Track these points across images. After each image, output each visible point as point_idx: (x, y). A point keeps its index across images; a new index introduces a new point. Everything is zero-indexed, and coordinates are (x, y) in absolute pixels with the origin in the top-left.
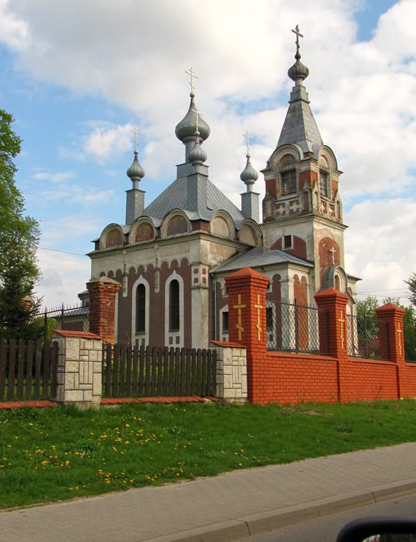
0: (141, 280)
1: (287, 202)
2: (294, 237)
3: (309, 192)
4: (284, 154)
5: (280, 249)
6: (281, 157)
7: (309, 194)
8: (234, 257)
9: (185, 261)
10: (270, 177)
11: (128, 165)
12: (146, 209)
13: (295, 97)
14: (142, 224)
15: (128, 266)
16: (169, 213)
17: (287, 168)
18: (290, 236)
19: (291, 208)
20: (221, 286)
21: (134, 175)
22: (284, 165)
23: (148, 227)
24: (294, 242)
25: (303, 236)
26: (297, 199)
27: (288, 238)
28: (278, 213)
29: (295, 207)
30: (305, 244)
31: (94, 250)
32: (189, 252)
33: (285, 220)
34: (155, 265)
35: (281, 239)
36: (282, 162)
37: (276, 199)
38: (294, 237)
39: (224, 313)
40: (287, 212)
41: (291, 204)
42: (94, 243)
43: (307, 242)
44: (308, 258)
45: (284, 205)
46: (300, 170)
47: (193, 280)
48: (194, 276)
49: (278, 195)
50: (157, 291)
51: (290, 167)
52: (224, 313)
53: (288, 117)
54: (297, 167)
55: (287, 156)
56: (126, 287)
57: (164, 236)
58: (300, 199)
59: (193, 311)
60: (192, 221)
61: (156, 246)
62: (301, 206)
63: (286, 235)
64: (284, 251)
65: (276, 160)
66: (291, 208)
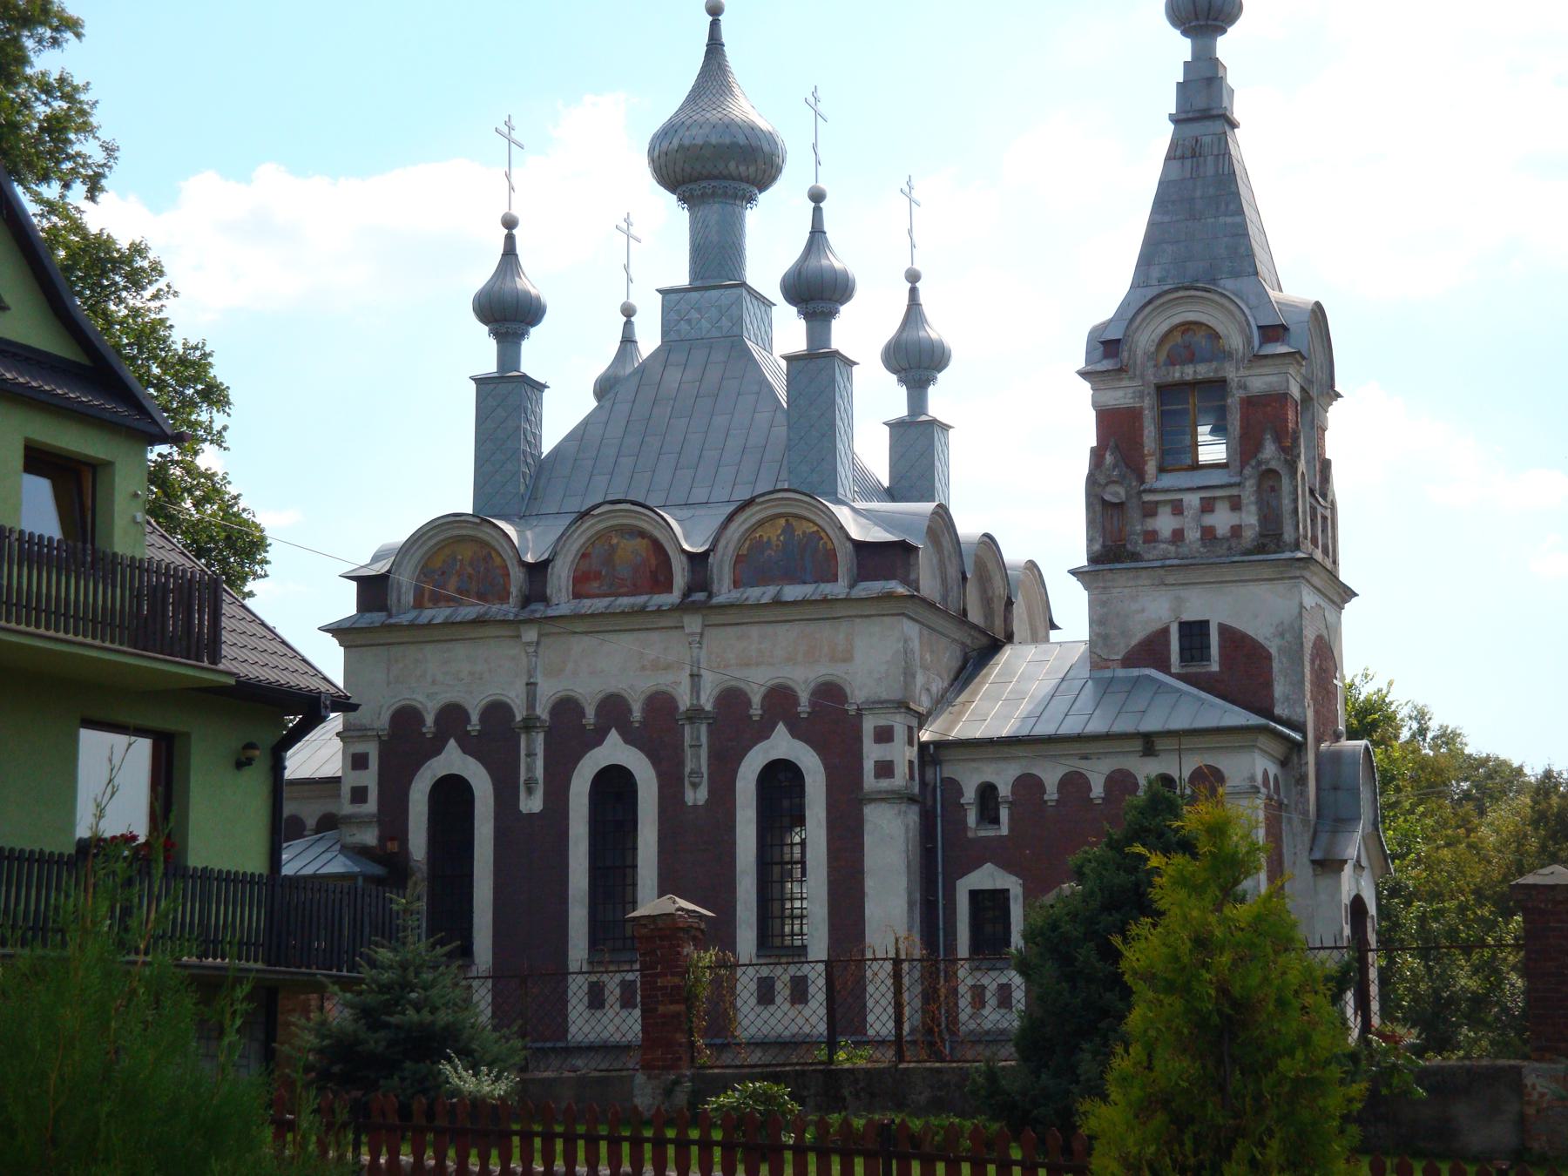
0: (614, 751)
1: (1192, 500)
2: (1220, 625)
3: (1283, 471)
4: (1177, 320)
5: (1164, 667)
6: (1165, 327)
7: (1285, 481)
8: (964, 675)
9: (830, 693)
10: (1120, 397)
11: (481, 273)
12: (556, 451)
13: (1200, 102)
14: (612, 529)
15: (549, 691)
16: (749, 503)
17: (1189, 372)
18: (1204, 625)
19: (1209, 520)
20: (961, 794)
21: (508, 313)
22: (1172, 361)
23: (640, 544)
24: (1221, 647)
25: (1259, 628)
26: (1235, 491)
27: (1194, 633)
28: (1151, 537)
29: (1222, 520)
30: (1269, 657)
31: (352, 609)
32: (848, 658)
33: (1187, 565)
34: (684, 701)
35: (1165, 631)
36: (1166, 348)
37: (1142, 482)
38: (1224, 630)
39: (974, 895)
40: (1193, 535)
41: (1207, 506)
42: (354, 584)
43: (1273, 651)
44: (1278, 711)
45: (1178, 508)
46: (1245, 387)
47: (869, 766)
48: (872, 753)
49: (1151, 467)
50: (696, 796)
51: (1203, 371)
52: (974, 895)
53: (1174, 176)
54: (1231, 373)
55: (1187, 327)
56: (539, 772)
57: (725, 592)
58: (1248, 494)
59: (870, 884)
60: (860, 546)
61: (693, 623)
62: (1250, 518)
63: (1186, 617)
64: (1179, 677)
65: (1146, 339)
66: (1209, 520)
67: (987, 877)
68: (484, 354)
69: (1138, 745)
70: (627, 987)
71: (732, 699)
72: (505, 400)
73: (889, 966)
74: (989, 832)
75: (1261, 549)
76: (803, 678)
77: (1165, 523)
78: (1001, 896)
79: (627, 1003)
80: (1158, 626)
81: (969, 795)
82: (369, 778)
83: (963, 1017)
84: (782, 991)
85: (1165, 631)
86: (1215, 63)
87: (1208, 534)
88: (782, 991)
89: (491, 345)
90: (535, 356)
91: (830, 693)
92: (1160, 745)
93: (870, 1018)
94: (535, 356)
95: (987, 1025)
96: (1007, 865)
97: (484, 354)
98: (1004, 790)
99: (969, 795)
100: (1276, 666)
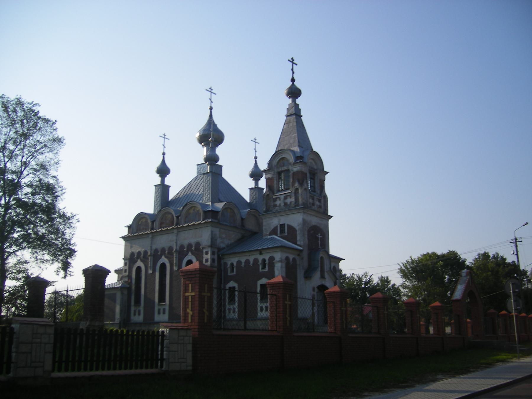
1: (282, 197)
5: (276, 235)
6: (278, 159)
9: (198, 244)
16: (186, 205)
27: (282, 226)
29: (288, 201)
30: (296, 231)
35: (277, 227)
38: (288, 226)
40: (282, 204)
43: (297, 229)
46: (292, 170)
51: (285, 168)
54: (290, 168)
62: (293, 199)
63: (281, 223)
67: (232, 284)
68: (157, 180)
69: (258, 253)
70: (267, 307)
71: (182, 247)
72: (163, 190)
73: (310, 302)
74: (232, 274)
75: (295, 206)
76: (193, 241)
77: (278, 203)
78: (234, 288)
79: (267, 310)
80: (275, 226)
81: (229, 266)
82: (127, 267)
83: (227, 315)
84: (162, 311)
85: (277, 227)
86: (297, 105)
87: (286, 204)
88: (162, 311)
89: (160, 179)
90: (168, 181)
91: (198, 244)
92: (263, 252)
93: (299, 312)
94: (168, 181)
95: (231, 317)
96: (236, 281)
97: (157, 180)
98: (235, 264)
99: (229, 266)
100: (298, 233)
